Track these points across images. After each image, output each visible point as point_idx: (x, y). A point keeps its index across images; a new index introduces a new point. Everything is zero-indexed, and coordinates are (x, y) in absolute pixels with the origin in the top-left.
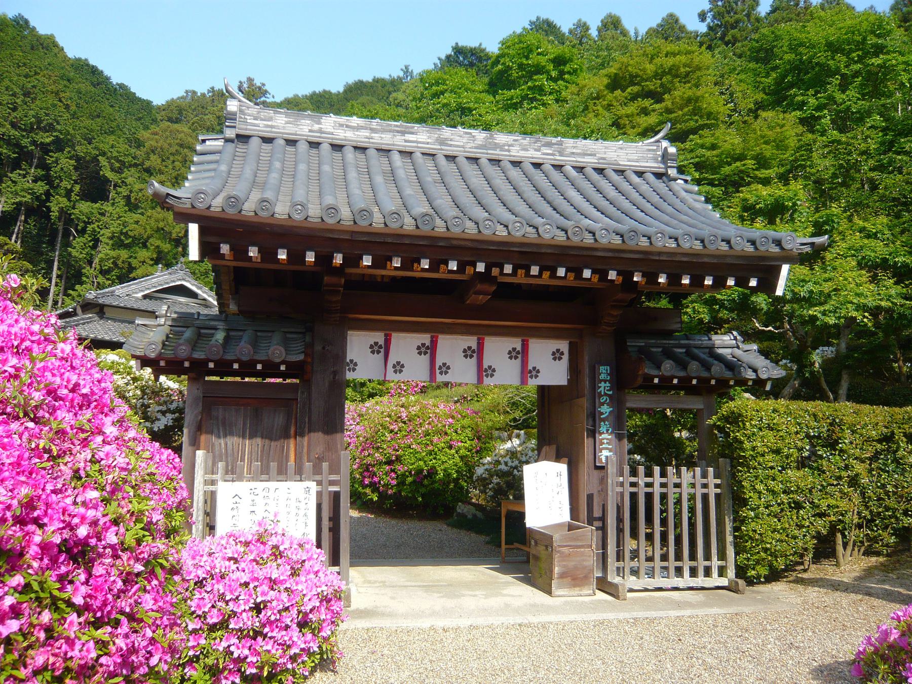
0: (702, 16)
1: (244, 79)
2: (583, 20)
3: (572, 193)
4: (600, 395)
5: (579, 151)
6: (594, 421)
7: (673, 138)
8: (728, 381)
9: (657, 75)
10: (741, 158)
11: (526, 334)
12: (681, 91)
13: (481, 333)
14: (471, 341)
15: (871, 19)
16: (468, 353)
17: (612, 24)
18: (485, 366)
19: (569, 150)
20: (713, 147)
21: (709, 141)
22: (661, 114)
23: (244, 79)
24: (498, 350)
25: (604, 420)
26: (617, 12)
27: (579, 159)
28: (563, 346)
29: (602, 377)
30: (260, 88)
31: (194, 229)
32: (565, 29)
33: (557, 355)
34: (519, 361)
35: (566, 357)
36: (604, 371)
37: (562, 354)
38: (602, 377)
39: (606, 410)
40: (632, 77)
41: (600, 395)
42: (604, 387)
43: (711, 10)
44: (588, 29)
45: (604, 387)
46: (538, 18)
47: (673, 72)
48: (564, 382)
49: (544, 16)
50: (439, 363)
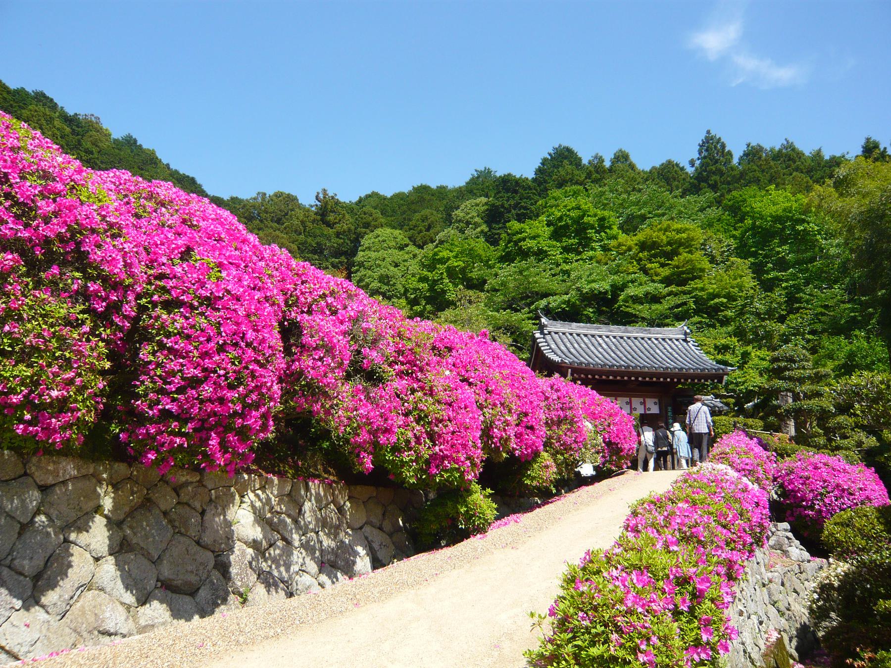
0: (692, 163)
1: (320, 191)
2: (600, 154)
3: (658, 351)
9: (669, 243)
10: (718, 296)
11: (644, 397)
12: (684, 256)
13: (630, 397)
14: (628, 399)
16: (641, 403)
17: (622, 157)
20: (702, 289)
21: (700, 286)
22: (673, 268)
23: (320, 191)
24: (636, 402)
26: (626, 149)
28: (656, 400)
30: (333, 198)
32: (585, 161)
36: (670, 409)
40: (654, 243)
42: (670, 414)
43: (698, 159)
44: (603, 161)
45: (670, 414)
46: (560, 146)
47: (680, 243)
49: (565, 144)
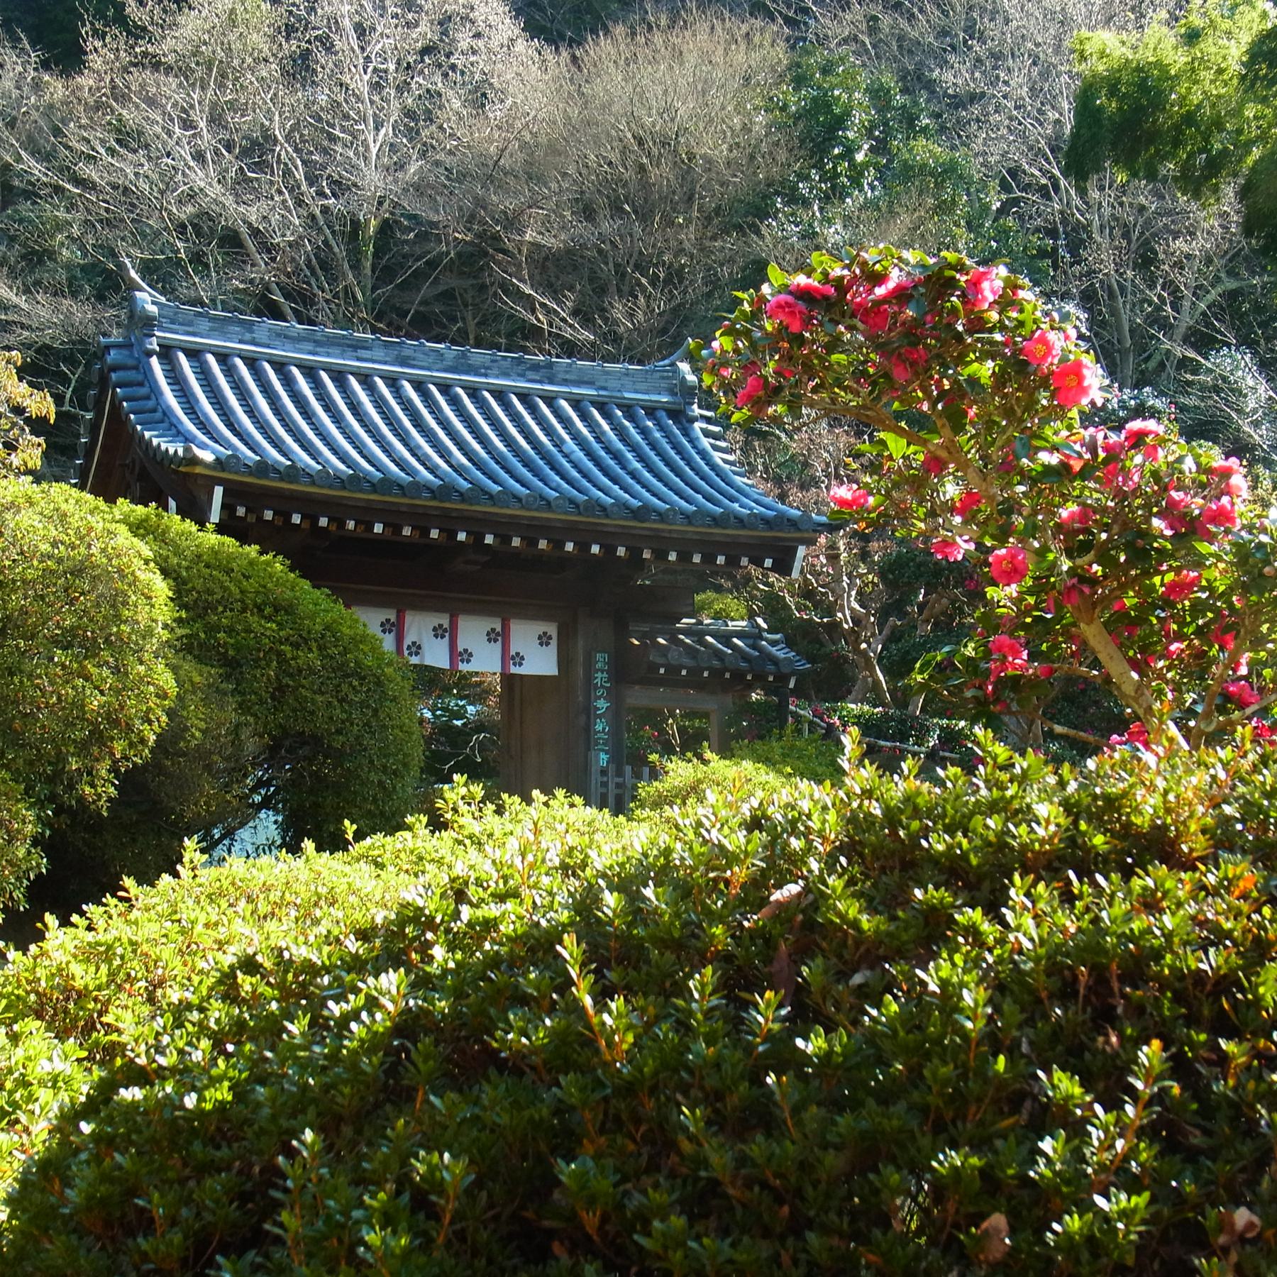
4: (596, 688)
5: (573, 377)
6: (589, 717)
7: (641, 910)
8: (743, 676)
15: (290, 1103)
18: (460, 649)
19: (561, 376)
25: (600, 716)
27: (575, 390)
28: (552, 629)
29: (599, 665)
31: (218, 491)
33: (544, 640)
34: (499, 643)
35: (554, 642)
36: (601, 660)
37: (550, 638)
38: (599, 665)
39: (602, 704)
41: (596, 688)
42: (600, 678)
48: (556, 673)
50: (408, 641)
